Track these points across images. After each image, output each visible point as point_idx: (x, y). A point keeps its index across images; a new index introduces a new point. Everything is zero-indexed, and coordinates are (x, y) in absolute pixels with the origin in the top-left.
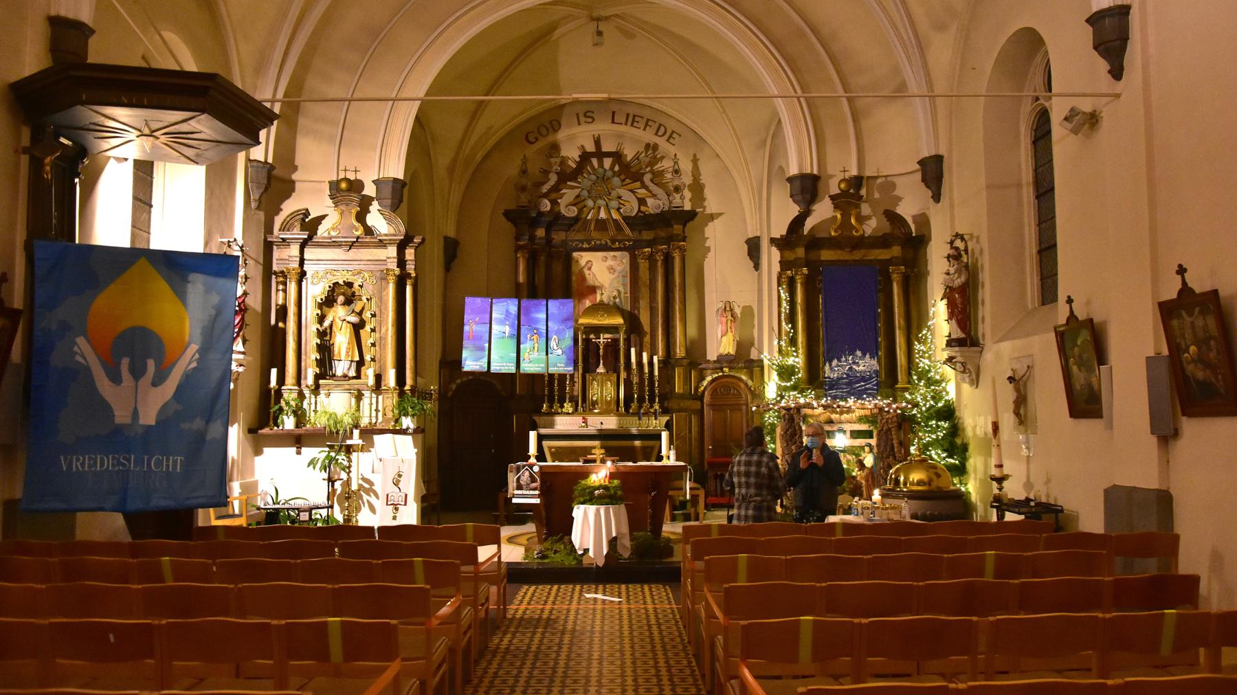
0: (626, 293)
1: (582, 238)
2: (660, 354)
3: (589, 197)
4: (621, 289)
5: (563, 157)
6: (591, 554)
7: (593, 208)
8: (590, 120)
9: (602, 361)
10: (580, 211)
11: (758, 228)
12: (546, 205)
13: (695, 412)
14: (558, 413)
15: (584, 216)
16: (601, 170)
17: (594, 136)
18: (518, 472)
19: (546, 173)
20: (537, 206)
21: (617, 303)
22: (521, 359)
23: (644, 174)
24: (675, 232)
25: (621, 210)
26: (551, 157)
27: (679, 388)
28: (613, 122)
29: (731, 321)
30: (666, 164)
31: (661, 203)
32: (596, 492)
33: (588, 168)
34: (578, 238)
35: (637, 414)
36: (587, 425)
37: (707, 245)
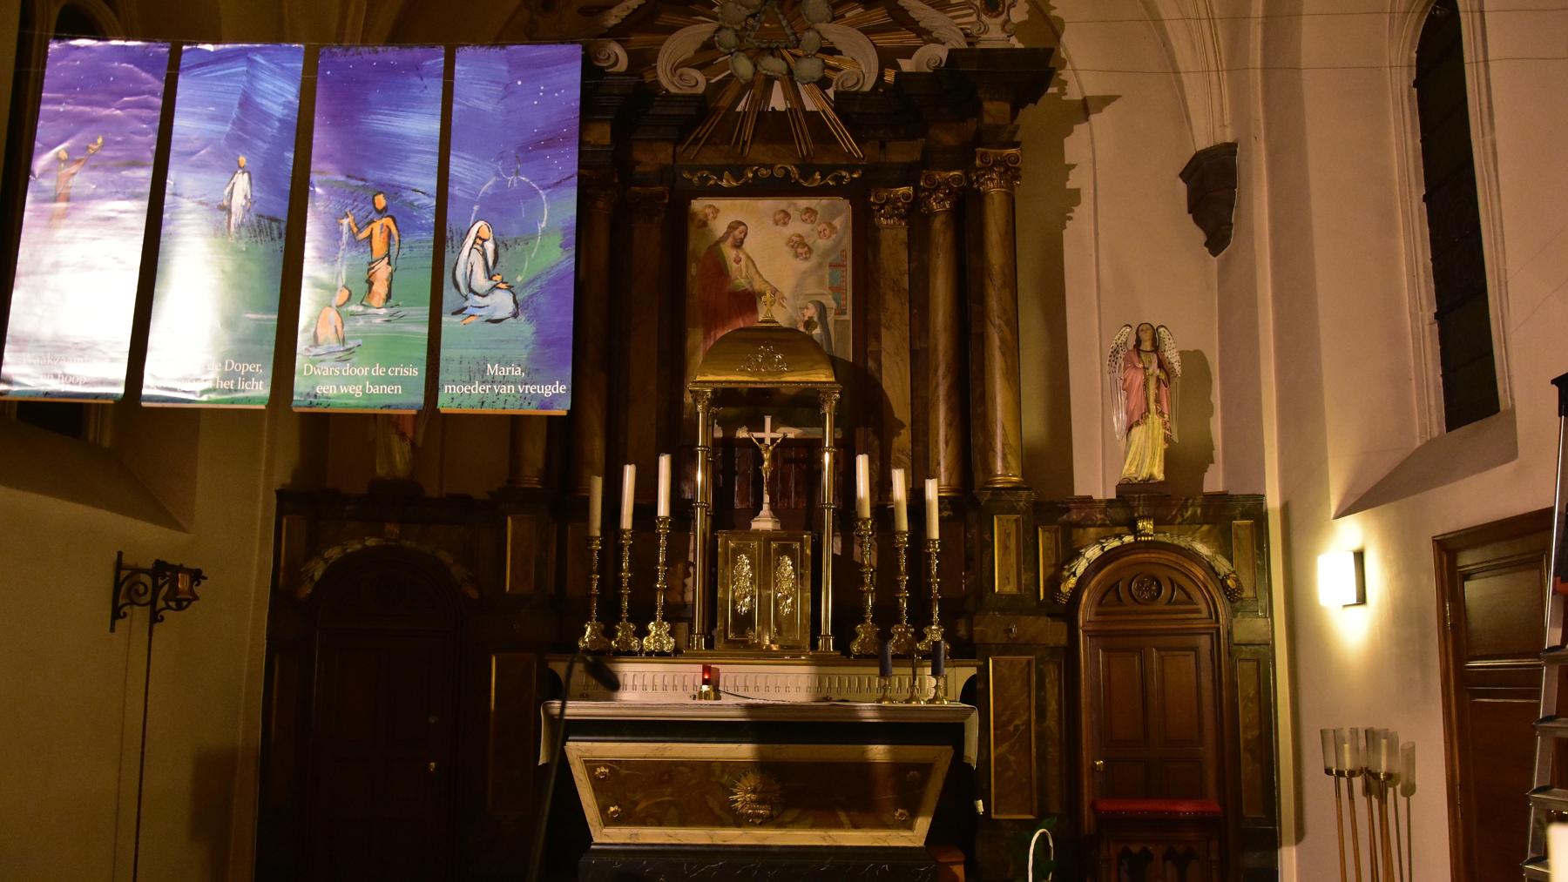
3: (739, 51)
4: (829, 302)
9: (767, 498)
11: (1227, 120)
14: (630, 654)
15: (725, 102)
27: (1005, 579)
29: (1158, 379)
34: (706, 162)
35: (877, 658)
36: (716, 690)
37: (1069, 185)
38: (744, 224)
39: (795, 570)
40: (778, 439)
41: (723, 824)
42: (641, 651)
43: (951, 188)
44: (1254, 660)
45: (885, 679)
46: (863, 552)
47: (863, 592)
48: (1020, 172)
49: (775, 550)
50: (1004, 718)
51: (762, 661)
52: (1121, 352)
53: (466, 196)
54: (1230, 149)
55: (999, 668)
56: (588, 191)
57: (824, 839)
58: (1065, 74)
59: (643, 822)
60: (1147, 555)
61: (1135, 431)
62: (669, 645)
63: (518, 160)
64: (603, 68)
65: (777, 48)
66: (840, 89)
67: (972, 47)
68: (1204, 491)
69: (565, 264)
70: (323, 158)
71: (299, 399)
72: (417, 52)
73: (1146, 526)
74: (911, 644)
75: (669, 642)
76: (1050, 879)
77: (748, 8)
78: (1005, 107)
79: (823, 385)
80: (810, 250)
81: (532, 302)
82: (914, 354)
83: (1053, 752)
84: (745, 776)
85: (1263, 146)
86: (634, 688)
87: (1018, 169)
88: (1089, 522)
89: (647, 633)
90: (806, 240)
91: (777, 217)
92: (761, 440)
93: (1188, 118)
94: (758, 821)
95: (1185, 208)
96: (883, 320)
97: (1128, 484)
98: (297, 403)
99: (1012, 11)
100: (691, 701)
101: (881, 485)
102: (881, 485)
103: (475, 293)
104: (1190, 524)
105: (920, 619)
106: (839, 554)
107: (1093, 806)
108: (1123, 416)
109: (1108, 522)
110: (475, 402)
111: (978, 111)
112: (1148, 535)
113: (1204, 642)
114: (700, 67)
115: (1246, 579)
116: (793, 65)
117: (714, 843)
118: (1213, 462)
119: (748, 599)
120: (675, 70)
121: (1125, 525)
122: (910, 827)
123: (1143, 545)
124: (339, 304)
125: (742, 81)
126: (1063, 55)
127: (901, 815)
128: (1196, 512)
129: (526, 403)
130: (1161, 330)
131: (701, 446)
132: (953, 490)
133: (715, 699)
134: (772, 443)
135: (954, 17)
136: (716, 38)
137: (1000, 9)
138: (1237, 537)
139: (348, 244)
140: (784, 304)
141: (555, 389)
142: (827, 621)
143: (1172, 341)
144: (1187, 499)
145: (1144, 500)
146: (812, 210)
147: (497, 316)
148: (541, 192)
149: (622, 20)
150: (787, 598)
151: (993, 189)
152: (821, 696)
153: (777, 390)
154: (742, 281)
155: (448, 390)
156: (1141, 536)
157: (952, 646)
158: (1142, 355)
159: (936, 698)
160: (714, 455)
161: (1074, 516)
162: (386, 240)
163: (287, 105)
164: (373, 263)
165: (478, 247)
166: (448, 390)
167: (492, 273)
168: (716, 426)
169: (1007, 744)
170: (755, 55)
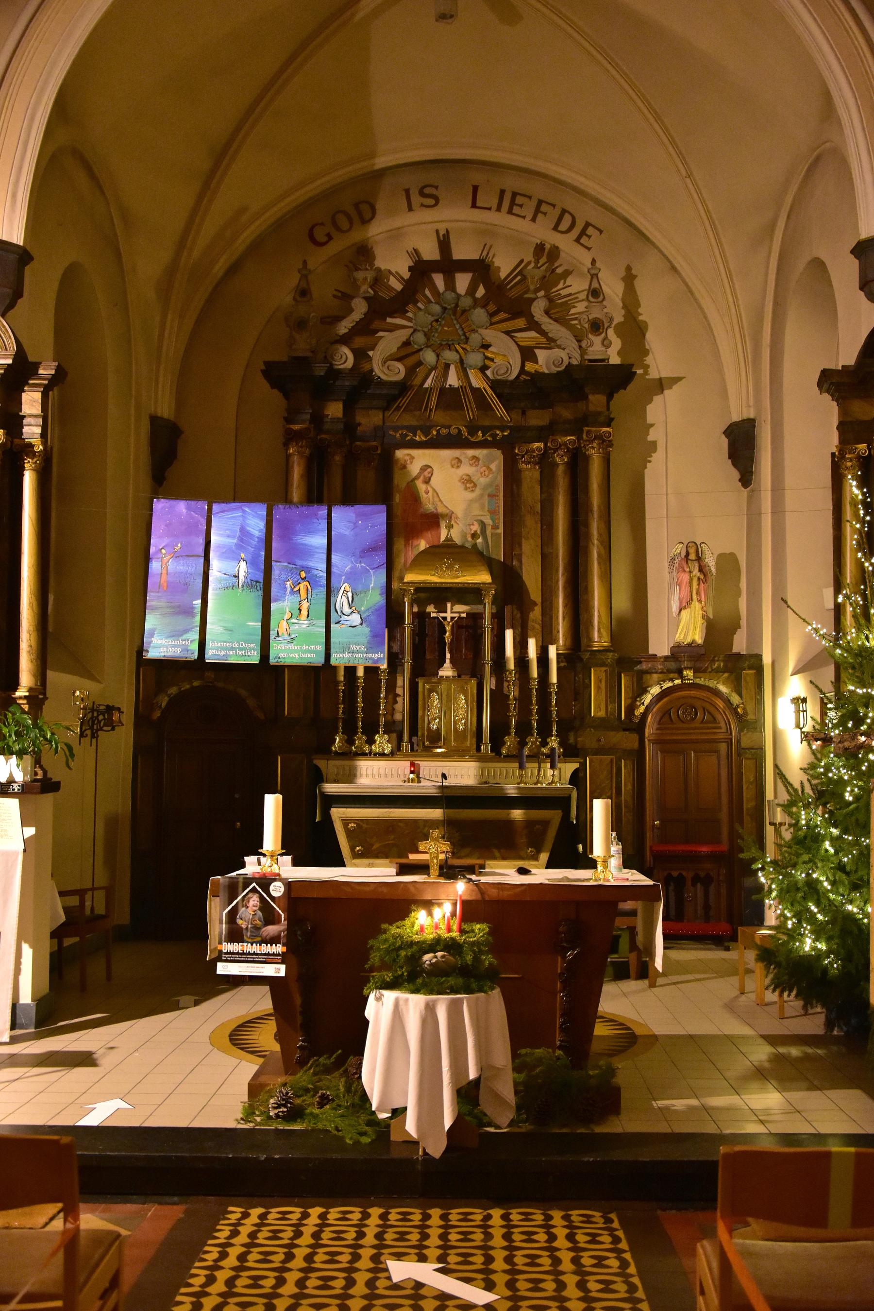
0: (495, 527)
1: (414, 423)
2: (561, 642)
3: (427, 347)
4: (488, 521)
5: (379, 270)
6: (411, 1126)
7: (435, 368)
8: (431, 202)
9: (448, 656)
10: (411, 371)
11: (751, 403)
12: (345, 358)
13: (627, 753)
14: (364, 754)
15: (417, 381)
16: (450, 296)
17: (437, 231)
18: (232, 896)
19: (346, 298)
20: (328, 359)
21: (480, 546)
22: (273, 634)
23: (533, 300)
24: (592, 408)
25: (488, 373)
26: (357, 269)
27: (598, 708)
28: (474, 205)
29: (699, 579)
30: (577, 285)
31: (563, 354)
32: (427, 957)
33: (427, 292)
34: (406, 424)
35: (517, 757)
36: (418, 777)
37: (650, 438)
42: (370, 753)
43: (568, 448)
44: (753, 759)
47: (509, 716)
60: (689, 692)
61: (683, 612)
63: (361, 557)
74: (539, 748)
77: (433, 316)
80: (475, 485)
85: (769, 427)
86: (367, 776)
89: (374, 742)
91: (453, 462)
97: (678, 646)
100: (402, 784)
101: (521, 646)
102: (521, 646)
105: (544, 733)
107: (651, 847)
112: (689, 679)
113: (723, 747)
114: (399, 360)
115: (750, 708)
116: (464, 357)
126: (647, 347)
127: (531, 852)
128: (719, 665)
134: (451, 620)
136: (412, 339)
137: (601, 331)
138: (746, 681)
142: (486, 732)
144: (714, 657)
151: (595, 454)
152: (484, 780)
157: (564, 750)
158: (689, 562)
159: (553, 782)
161: (644, 666)
163: (260, 531)
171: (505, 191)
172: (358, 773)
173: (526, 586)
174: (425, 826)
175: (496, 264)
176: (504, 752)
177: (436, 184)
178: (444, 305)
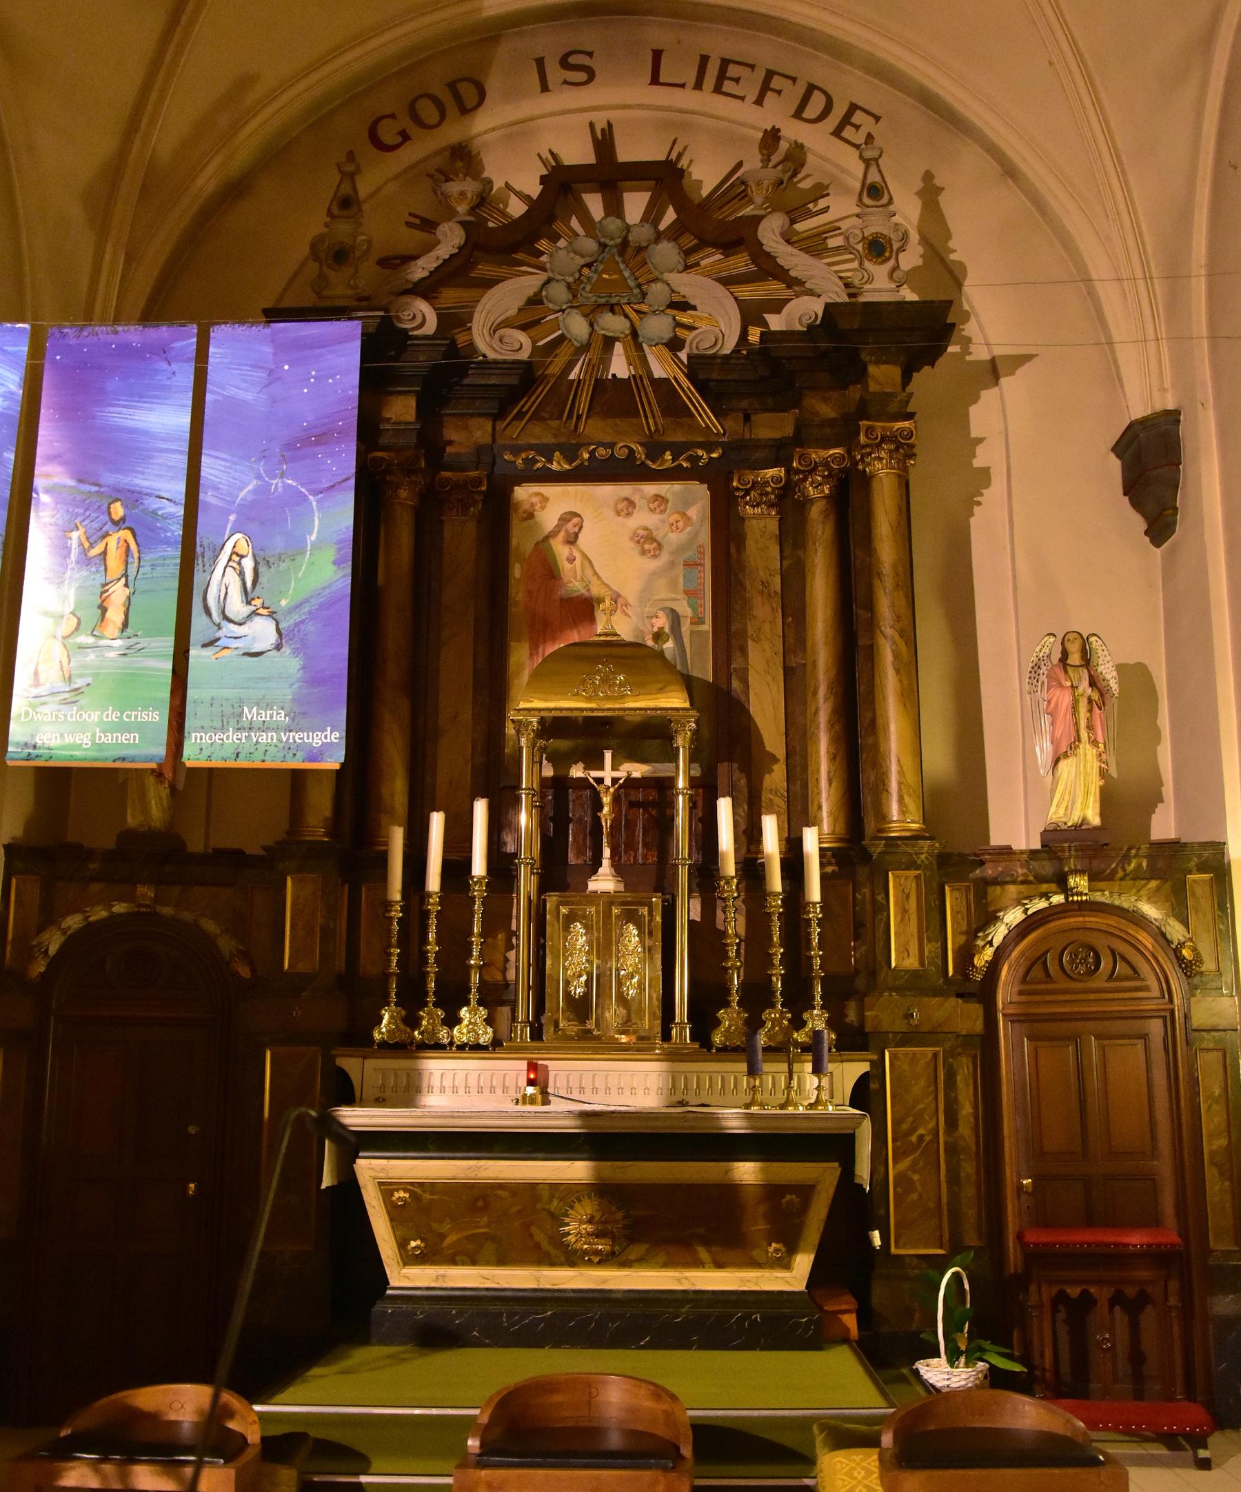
0: (698, 621)
1: (548, 439)
2: (826, 827)
4: (684, 609)
8: (582, 76)
9: (607, 852)
11: (1167, 384)
13: (967, 1040)
14: (438, 1047)
15: (555, 369)
17: (592, 125)
26: (448, 180)
27: (904, 951)
28: (655, 80)
29: (1090, 700)
33: (574, 223)
35: (744, 1051)
37: (977, 463)
38: (579, 516)
39: (642, 942)
40: (620, 779)
41: (552, 1263)
42: (451, 1043)
43: (830, 470)
45: (755, 1080)
46: (726, 918)
47: (726, 969)
48: (915, 450)
49: (618, 917)
50: (905, 1126)
51: (497, 1155)
52: (1043, 667)
53: (220, 504)
54: (1172, 417)
55: (897, 1063)
56: (388, 478)
57: (679, 1280)
58: (970, 329)
59: (452, 1261)
60: (1081, 919)
61: (1062, 764)
62: (486, 1035)
64: (406, 331)
65: (618, 304)
66: (695, 352)
67: (853, 300)
68: (1153, 838)
69: (340, 585)
70: (51, 459)
71: (14, 750)
72: (163, 332)
73: (1079, 882)
74: (787, 1033)
75: (485, 1033)
76: (966, 1330)
77: (582, 256)
78: (895, 372)
79: (674, 713)
80: (660, 546)
81: (298, 631)
82: (788, 672)
83: (968, 1168)
84: (572, 1207)
85: (1211, 414)
86: (442, 1090)
87: (912, 446)
88: (1008, 879)
89: (459, 1021)
90: (655, 534)
91: (620, 506)
92: (600, 781)
93: (1120, 379)
94: (596, 1259)
95: (1120, 490)
96: (750, 632)
97: (1055, 830)
98: (13, 755)
99: (901, 255)
101: (749, 835)
102: (749, 835)
103: (230, 621)
104: (1134, 879)
105: (798, 1002)
106: (699, 919)
107: (1020, 1237)
108: (1048, 746)
109: (1031, 878)
110: (229, 753)
111: (861, 375)
113: (1155, 1027)
114: (524, 328)
115: (1205, 949)
116: (637, 324)
117: (542, 1287)
118: (1162, 801)
119: (583, 979)
120: (494, 332)
121: (1053, 882)
122: (787, 1266)
123: (1076, 907)
124: (65, 634)
125: (575, 343)
126: (966, 307)
127: (776, 1251)
128: (1140, 865)
129: (291, 754)
130: (1093, 639)
131: (526, 789)
132: (839, 840)
133: (543, 1104)
135: (830, 264)
136: (544, 293)
137: (887, 254)
139: (77, 562)
140: (629, 612)
141: (326, 737)
143: (1106, 653)
144: (1130, 849)
145: (1076, 850)
146: (660, 496)
147: (257, 648)
148: (311, 497)
149: (431, 272)
150: (633, 977)
151: (882, 470)
152: (678, 1098)
153: (619, 719)
154: (577, 584)
155: (196, 739)
156: (1073, 895)
157: (838, 1035)
158: (1070, 670)
159: (818, 1102)
160: (543, 797)
161: (989, 871)
162: (124, 556)
164: (106, 584)
165: (235, 565)
166: (196, 739)
167: (250, 597)
168: (545, 762)
169: (909, 1159)
170: (591, 314)
171: (708, 57)
172: (425, 1084)
173: (756, 725)
174: (552, 1197)
175: (695, 177)
176: (717, 1040)
177: (589, 50)
178: (602, 240)
